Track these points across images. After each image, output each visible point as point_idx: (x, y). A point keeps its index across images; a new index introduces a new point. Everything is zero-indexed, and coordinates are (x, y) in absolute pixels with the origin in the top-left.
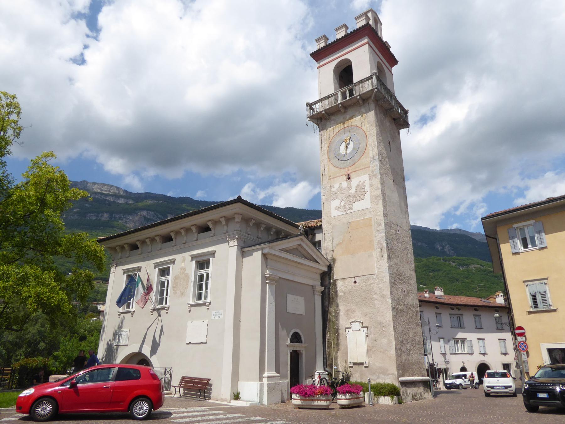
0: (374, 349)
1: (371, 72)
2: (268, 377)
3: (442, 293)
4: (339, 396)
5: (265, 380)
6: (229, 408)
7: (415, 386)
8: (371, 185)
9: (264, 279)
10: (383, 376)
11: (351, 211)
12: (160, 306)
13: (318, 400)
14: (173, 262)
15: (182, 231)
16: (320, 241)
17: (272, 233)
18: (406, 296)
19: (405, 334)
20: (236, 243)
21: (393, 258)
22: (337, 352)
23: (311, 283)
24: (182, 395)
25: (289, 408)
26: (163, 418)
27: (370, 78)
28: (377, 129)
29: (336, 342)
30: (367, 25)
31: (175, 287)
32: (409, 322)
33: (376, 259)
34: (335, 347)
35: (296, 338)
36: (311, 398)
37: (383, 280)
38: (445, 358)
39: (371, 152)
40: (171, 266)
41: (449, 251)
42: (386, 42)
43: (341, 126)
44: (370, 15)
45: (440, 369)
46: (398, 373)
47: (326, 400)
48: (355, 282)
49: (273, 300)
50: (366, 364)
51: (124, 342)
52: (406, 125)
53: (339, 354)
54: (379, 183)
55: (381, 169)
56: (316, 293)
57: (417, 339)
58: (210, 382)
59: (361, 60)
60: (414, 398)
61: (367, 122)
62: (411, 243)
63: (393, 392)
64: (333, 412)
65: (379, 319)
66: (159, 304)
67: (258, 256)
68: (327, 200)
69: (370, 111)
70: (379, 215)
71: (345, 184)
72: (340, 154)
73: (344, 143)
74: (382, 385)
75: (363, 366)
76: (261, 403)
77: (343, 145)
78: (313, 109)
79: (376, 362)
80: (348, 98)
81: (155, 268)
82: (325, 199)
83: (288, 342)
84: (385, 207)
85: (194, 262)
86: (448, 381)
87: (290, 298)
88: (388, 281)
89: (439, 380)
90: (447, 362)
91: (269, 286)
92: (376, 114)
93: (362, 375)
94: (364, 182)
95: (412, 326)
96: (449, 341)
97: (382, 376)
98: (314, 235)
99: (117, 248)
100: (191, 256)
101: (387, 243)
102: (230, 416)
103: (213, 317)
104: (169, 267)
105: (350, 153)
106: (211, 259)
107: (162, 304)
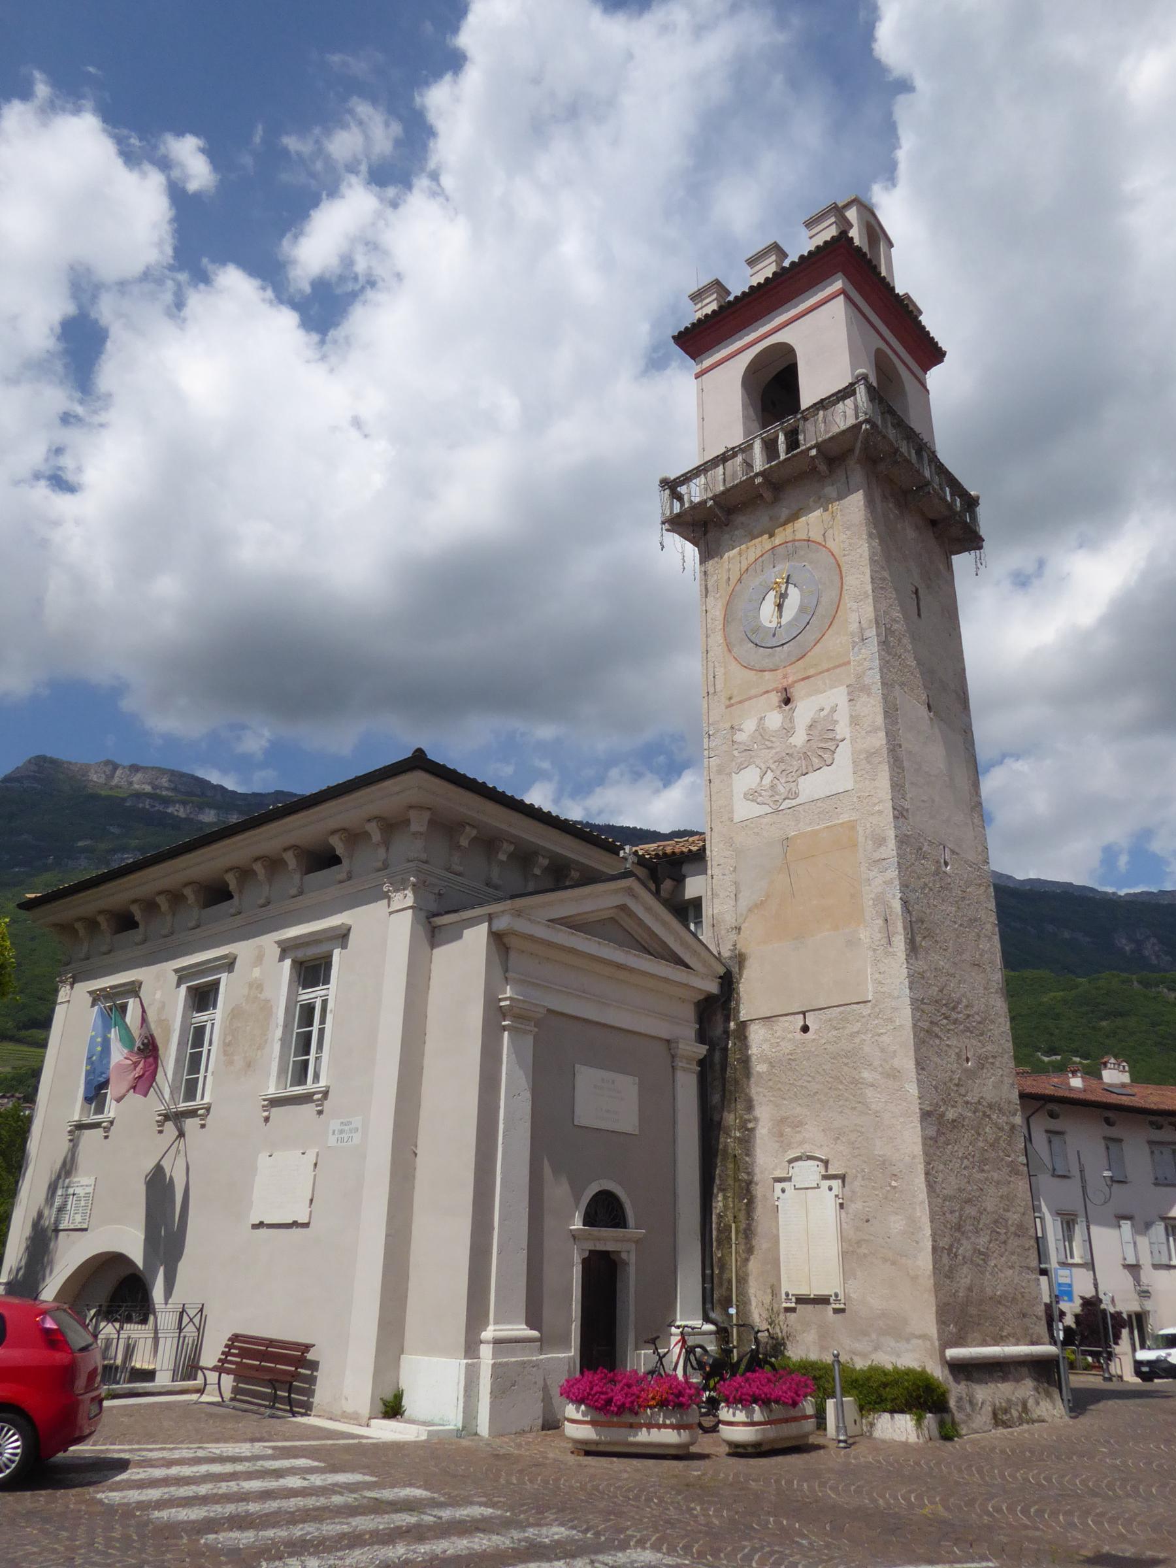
1: (853, 371)
2: (497, 1342)
3: (1125, 1078)
4: (725, 1413)
5: (486, 1351)
6: (347, 1449)
7: (1004, 1379)
8: (855, 721)
9: (495, 1014)
10: (892, 1343)
11: (794, 803)
12: (183, 1106)
13: (649, 1426)
14: (229, 964)
15: (258, 867)
16: (700, 898)
17: (537, 871)
18: (971, 1074)
19: (969, 1201)
20: (410, 901)
21: (927, 951)
22: (747, 1260)
23: (662, 1029)
24: (228, 1395)
25: (555, 1451)
26: (90, 1484)
27: (847, 393)
28: (871, 547)
29: (743, 1226)
30: (842, 240)
31: (229, 1044)
32: (984, 1161)
33: (871, 953)
35: (605, 1210)
36: (628, 1418)
38: (1137, 1280)
39: (853, 617)
40: (224, 977)
41: (1158, 957)
42: (907, 296)
43: (763, 544)
44: (852, 214)
45: (1119, 1314)
46: (940, 1332)
47: (677, 1427)
48: (805, 1029)
49: (523, 1083)
50: (837, 1300)
51: (78, 1218)
52: (971, 540)
53: (753, 1266)
54: (879, 710)
55: (885, 667)
56: (680, 1064)
57: (1014, 1217)
58: (310, 1356)
59: (825, 344)
60: (999, 1418)
61: (842, 528)
62: (992, 905)
63: (919, 1396)
64: (695, 1470)
66: (185, 1100)
67: (476, 937)
69: (850, 492)
71: (775, 719)
72: (758, 629)
73: (772, 594)
74: (885, 1373)
75: (830, 1308)
76: (468, 1428)
77: (771, 597)
78: (680, 498)
79: (869, 1295)
80: (783, 457)
81: (178, 985)
82: (714, 769)
83: (577, 1224)
84: (897, 787)
85: (288, 963)
86: (1144, 1355)
87: (587, 1078)
88: (909, 1024)
89: (1117, 1349)
90: (1145, 1294)
92: (870, 502)
93: (824, 1335)
94: (834, 710)
95: (996, 1176)
96: (1148, 1225)
98: (680, 881)
99: (78, 925)
100: (279, 943)
101: (905, 903)
102: (341, 1478)
103: (332, 1141)
104: (216, 985)
105: (789, 623)
106: (337, 953)
107: (194, 1100)
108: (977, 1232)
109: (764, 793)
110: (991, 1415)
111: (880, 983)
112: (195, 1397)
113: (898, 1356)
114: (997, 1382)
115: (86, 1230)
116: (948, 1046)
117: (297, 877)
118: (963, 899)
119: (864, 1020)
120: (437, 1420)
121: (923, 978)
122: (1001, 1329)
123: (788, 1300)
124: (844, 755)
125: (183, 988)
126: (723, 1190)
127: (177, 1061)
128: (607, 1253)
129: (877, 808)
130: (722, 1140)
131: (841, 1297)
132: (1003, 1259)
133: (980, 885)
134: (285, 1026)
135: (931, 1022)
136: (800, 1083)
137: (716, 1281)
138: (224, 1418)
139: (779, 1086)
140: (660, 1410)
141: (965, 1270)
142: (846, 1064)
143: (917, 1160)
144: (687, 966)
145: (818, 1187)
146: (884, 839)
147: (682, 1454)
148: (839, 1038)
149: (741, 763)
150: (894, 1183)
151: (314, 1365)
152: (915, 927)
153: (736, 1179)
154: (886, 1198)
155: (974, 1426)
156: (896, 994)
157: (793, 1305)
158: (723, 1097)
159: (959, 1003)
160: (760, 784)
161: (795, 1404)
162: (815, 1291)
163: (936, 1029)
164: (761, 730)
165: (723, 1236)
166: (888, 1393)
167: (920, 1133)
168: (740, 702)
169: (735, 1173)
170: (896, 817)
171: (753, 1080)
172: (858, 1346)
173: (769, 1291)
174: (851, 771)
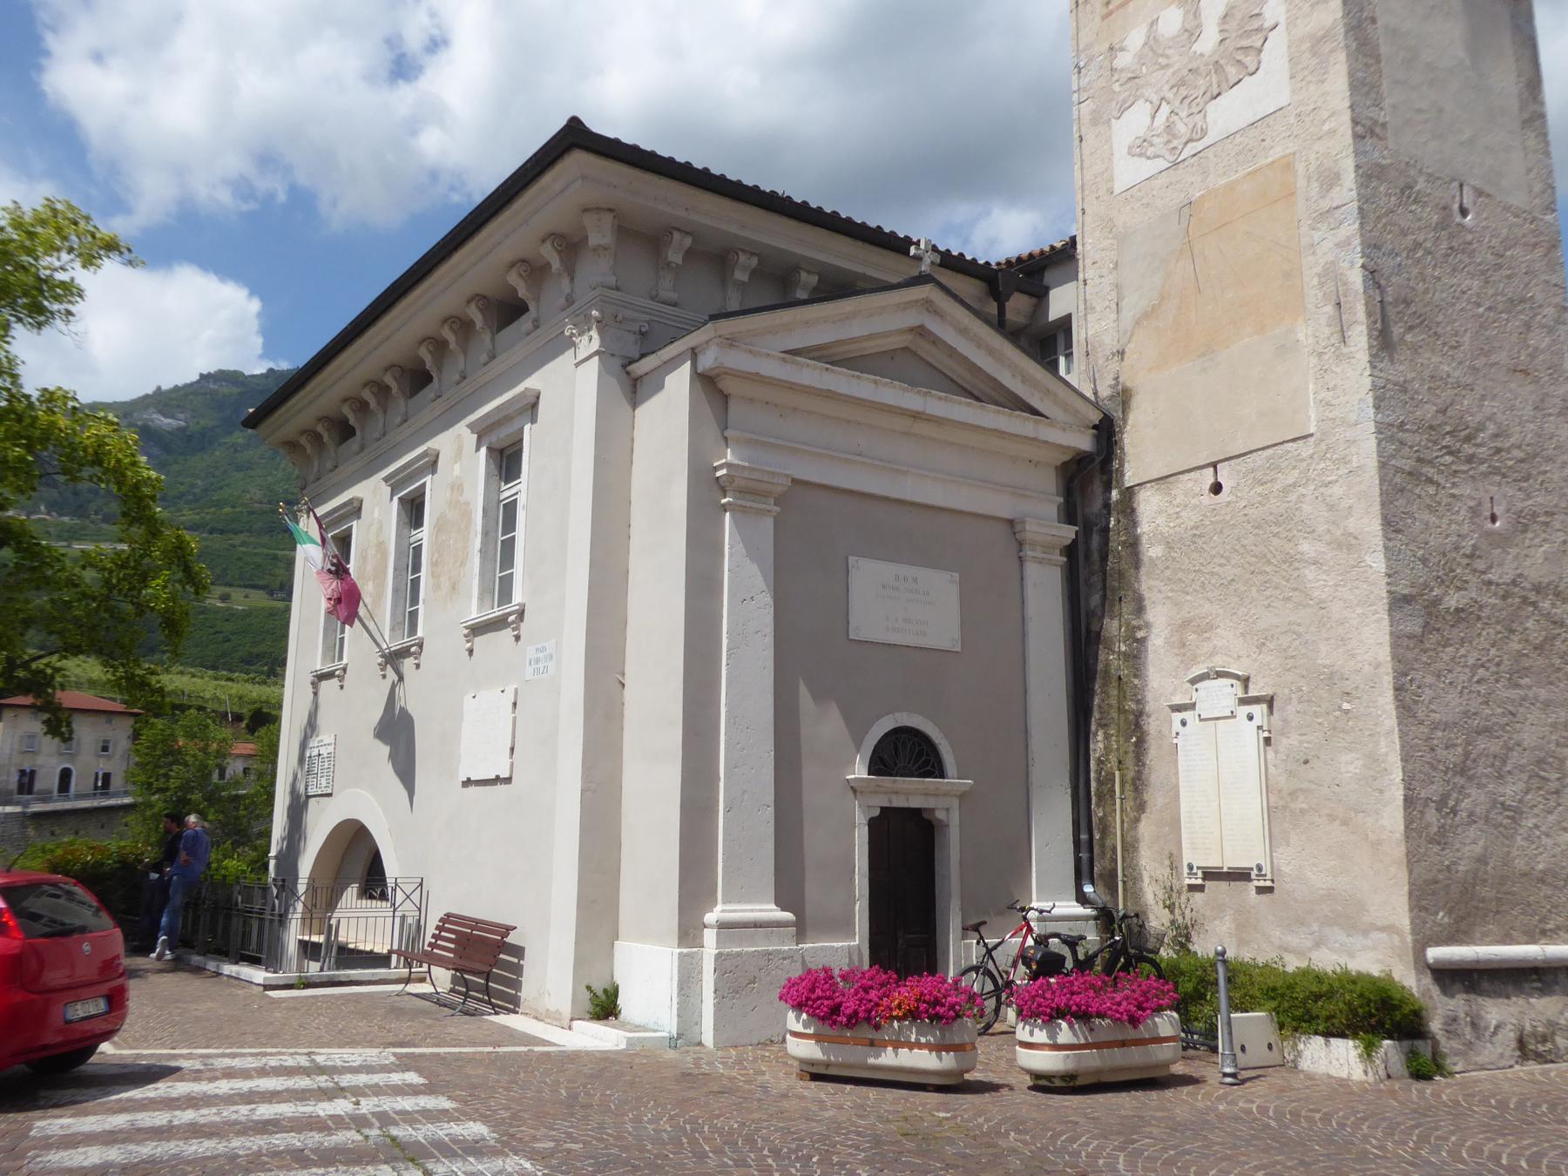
0: (1300, 804)
2: (723, 926)
5: (710, 937)
7: (1544, 991)
11: (1199, 146)
13: (897, 1045)
18: (1502, 541)
19: (1485, 731)
20: (596, 345)
21: (1415, 349)
22: (1137, 820)
23: (1001, 506)
29: (1131, 774)
33: (1314, 360)
34: (1129, 793)
35: (905, 753)
36: (867, 1032)
37: (1345, 460)
40: (428, 479)
47: (938, 1048)
48: (1217, 488)
50: (1261, 875)
53: (1146, 829)
56: (1028, 552)
60: (1524, 1050)
63: (1376, 1015)
65: (1326, 655)
68: (1095, 122)
70: (1333, 132)
74: (1319, 978)
76: (685, 1037)
79: (1306, 866)
82: (1086, 119)
83: (859, 771)
84: (1364, 87)
85: (484, 450)
88: (1372, 463)
91: (732, 517)
93: (1244, 926)
97: (1338, 936)
101: (1372, 275)
106: (527, 428)
108: (1500, 777)
109: (1156, 140)
110: (1514, 1044)
111: (1328, 404)
112: (400, 987)
113: (1352, 955)
114: (1531, 995)
115: (330, 795)
116: (1453, 496)
117: (487, 337)
118: (1498, 267)
120: (651, 1026)
121: (1405, 391)
122: (1544, 920)
123: (1191, 874)
124: (1276, 51)
125: (396, 499)
126: (1102, 726)
127: (395, 591)
128: (917, 812)
129: (1326, 127)
130: (1102, 657)
131: (1267, 870)
132: (1551, 818)
133: (1535, 245)
134: (485, 533)
135: (1419, 460)
136: (1209, 568)
137: (1096, 850)
138: (416, 1014)
139: (1180, 575)
141: (1472, 832)
143: (1382, 670)
144: (1035, 412)
145: (1233, 716)
146: (1337, 176)
147: (953, 1085)
148: (1266, 497)
149: (1124, 101)
150: (1346, 706)
151: (518, 951)
152: (1391, 312)
153: (1121, 710)
154: (1334, 728)
155: (1480, 1059)
156: (1353, 417)
157: (1199, 882)
158: (1104, 597)
159: (1478, 430)
160: (1151, 128)
161: (1134, 1021)
162: (1230, 862)
163: (1429, 471)
164: (1153, 45)
165: (1105, 789)
167: (1387, 629)
168: (1122, 6)
170: (1358, 137)
171: (1143, 570)
172: (1292, 940)
173: (1167, 862)
174: (1287, 75)
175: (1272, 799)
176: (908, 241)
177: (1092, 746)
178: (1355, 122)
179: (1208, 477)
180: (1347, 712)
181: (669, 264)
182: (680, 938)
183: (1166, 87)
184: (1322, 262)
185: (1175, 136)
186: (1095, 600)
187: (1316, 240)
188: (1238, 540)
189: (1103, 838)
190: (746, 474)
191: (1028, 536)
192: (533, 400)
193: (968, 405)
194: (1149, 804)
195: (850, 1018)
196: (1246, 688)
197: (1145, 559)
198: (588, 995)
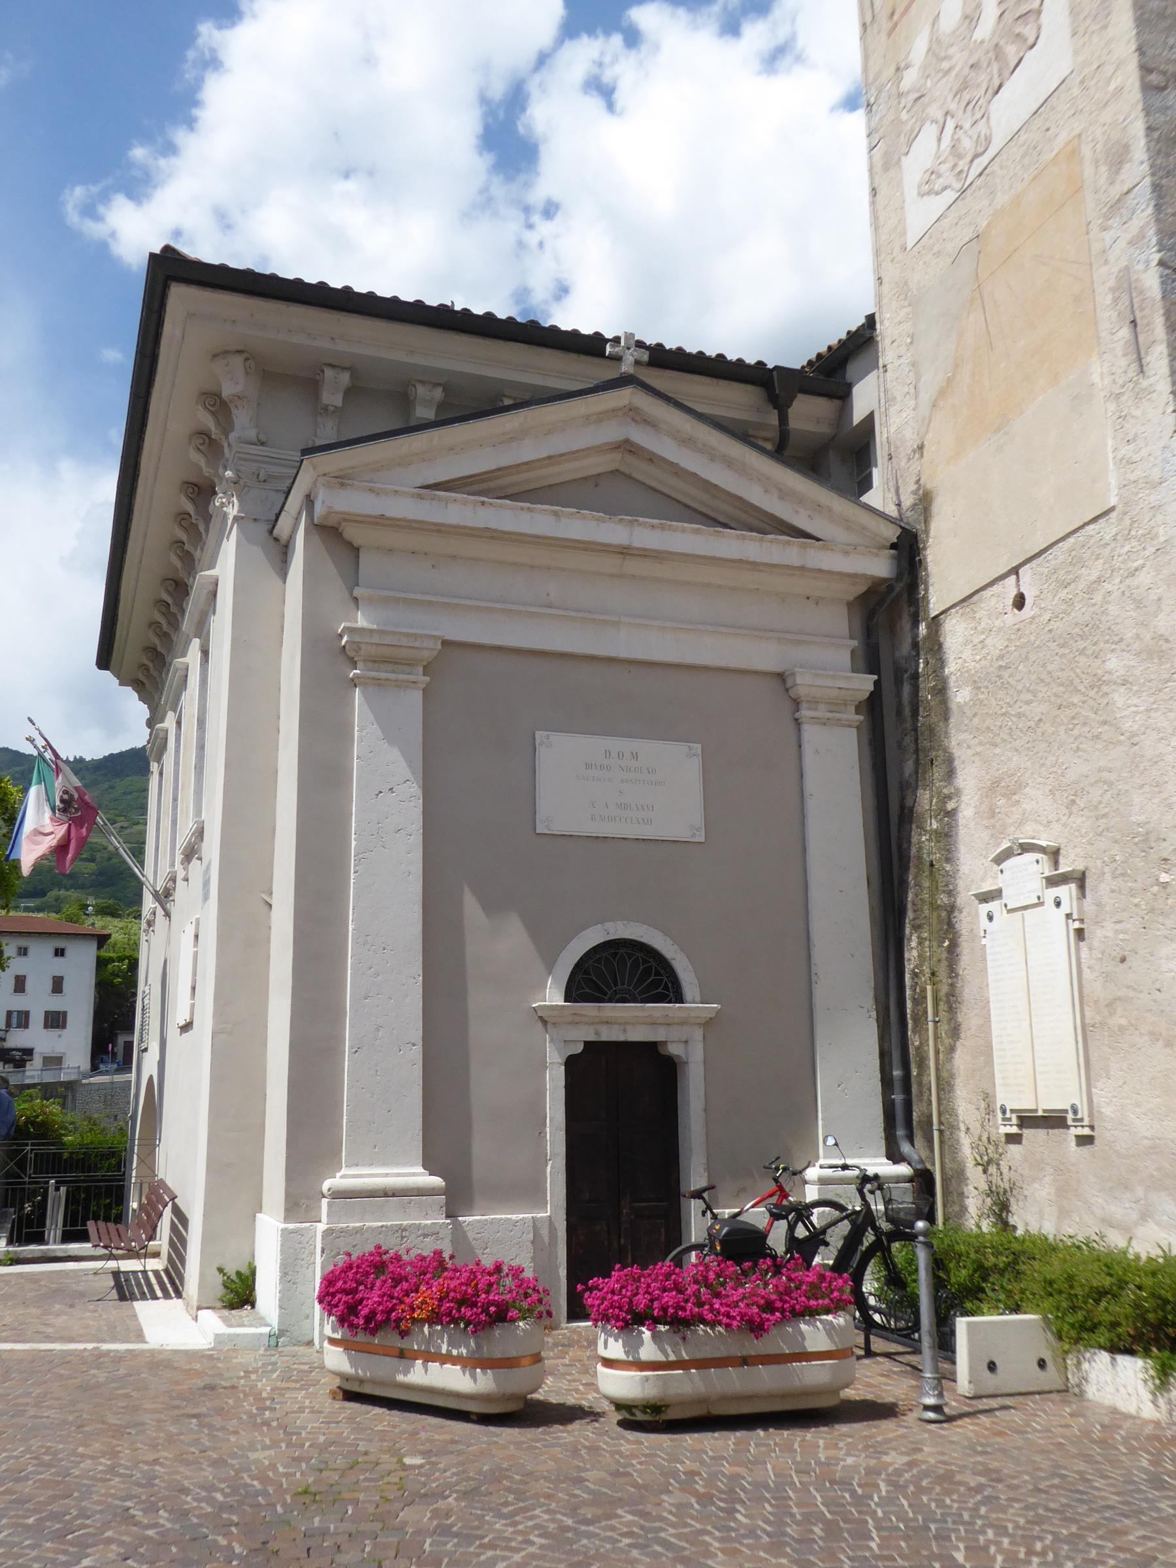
11: (984, 160)
13: (430, 1357)
22: (952, 1049)
23: (764, 656)
29: (944, 989)
35: (620, 971)
37: (1151, 535)
47: (471, 1363)
48: (1020, 602)
53: (962, 1061)
56: (805, 713)
70: (1119, 90)
83: (553, 996)
91: (362, 692)
119: (1107, 551)
126: (917, 928)
129: (1112, 87)
130: (914, 840)
131: (1083, 1113)
140: (443, 1330)
142: (1082, 652)
146: (1126, 148)
147: (526, 1413)
148: (1069, 602)
149: (912, 130)
150: (1164, 878)
153: (934, 907)
154: (1152, 910)
157: (1014, 1130)
160: (937, 155)
162: (1047, 1103)
166: (1104, 1311)
169: (932, 896)
170: (1148, 89)
171: (952, 720)
175: (1089, 1014)
176: (598, 339)
177: (906, 955)
178: (1145, 69)
179: (1009, 588)
180: (1165, 885)
181: (326, 408)
182: (287, 1210)
183: (950, 97)
184: (1115, 270)
185: (960, 157)
186: (909, 766)
187: (1108, 243)
188: (1044, 665)
189: (920, 1075)
190: (376, 639)
191: (801, 691)
192: (211, 588)
193: (697, 532)
194: (963, 1027)
195: (368, 1319)
196: (1056, 864)
197: (953, 706)
198: (220, 1278)
